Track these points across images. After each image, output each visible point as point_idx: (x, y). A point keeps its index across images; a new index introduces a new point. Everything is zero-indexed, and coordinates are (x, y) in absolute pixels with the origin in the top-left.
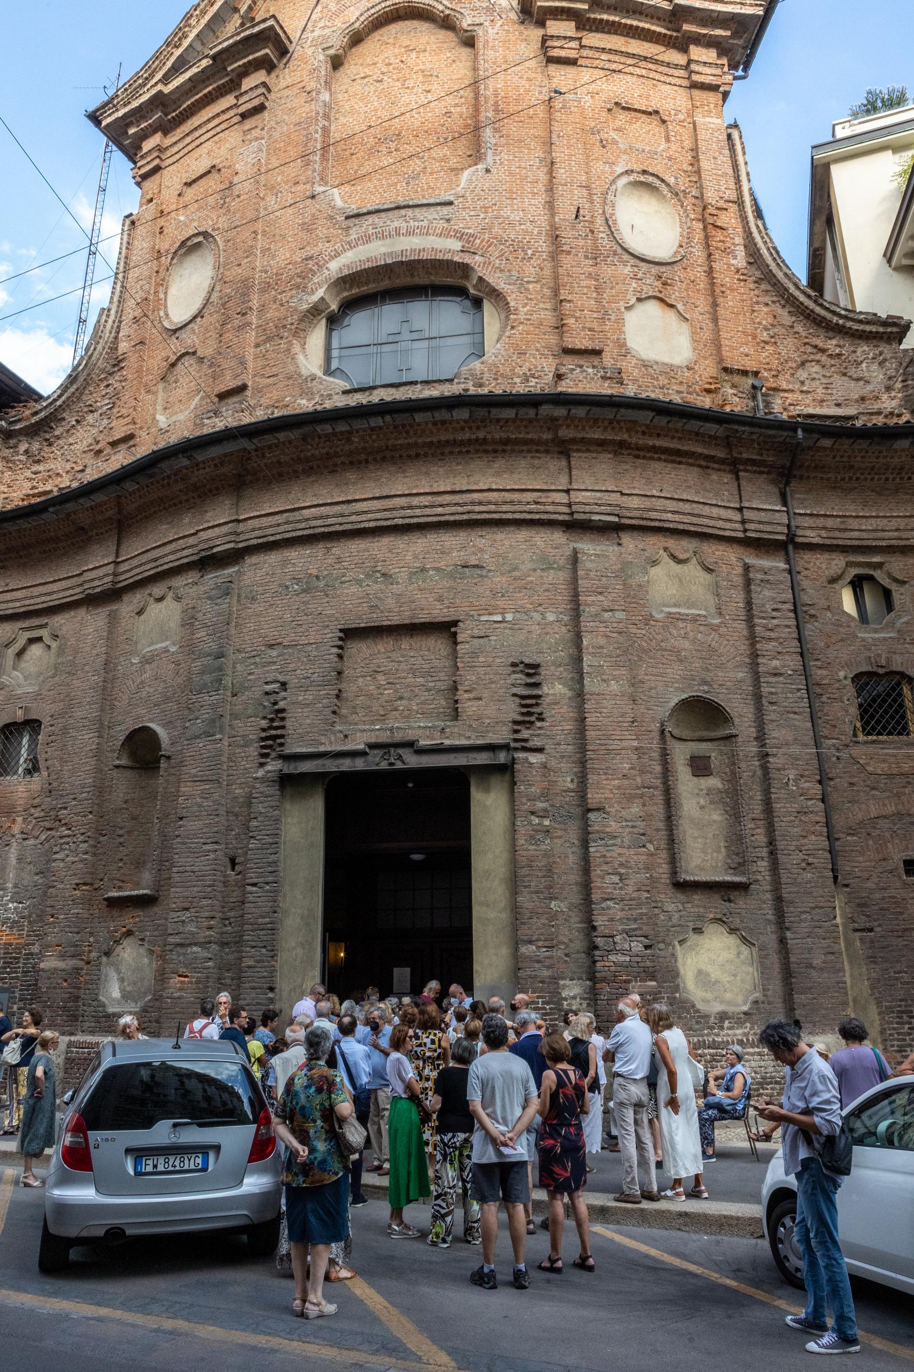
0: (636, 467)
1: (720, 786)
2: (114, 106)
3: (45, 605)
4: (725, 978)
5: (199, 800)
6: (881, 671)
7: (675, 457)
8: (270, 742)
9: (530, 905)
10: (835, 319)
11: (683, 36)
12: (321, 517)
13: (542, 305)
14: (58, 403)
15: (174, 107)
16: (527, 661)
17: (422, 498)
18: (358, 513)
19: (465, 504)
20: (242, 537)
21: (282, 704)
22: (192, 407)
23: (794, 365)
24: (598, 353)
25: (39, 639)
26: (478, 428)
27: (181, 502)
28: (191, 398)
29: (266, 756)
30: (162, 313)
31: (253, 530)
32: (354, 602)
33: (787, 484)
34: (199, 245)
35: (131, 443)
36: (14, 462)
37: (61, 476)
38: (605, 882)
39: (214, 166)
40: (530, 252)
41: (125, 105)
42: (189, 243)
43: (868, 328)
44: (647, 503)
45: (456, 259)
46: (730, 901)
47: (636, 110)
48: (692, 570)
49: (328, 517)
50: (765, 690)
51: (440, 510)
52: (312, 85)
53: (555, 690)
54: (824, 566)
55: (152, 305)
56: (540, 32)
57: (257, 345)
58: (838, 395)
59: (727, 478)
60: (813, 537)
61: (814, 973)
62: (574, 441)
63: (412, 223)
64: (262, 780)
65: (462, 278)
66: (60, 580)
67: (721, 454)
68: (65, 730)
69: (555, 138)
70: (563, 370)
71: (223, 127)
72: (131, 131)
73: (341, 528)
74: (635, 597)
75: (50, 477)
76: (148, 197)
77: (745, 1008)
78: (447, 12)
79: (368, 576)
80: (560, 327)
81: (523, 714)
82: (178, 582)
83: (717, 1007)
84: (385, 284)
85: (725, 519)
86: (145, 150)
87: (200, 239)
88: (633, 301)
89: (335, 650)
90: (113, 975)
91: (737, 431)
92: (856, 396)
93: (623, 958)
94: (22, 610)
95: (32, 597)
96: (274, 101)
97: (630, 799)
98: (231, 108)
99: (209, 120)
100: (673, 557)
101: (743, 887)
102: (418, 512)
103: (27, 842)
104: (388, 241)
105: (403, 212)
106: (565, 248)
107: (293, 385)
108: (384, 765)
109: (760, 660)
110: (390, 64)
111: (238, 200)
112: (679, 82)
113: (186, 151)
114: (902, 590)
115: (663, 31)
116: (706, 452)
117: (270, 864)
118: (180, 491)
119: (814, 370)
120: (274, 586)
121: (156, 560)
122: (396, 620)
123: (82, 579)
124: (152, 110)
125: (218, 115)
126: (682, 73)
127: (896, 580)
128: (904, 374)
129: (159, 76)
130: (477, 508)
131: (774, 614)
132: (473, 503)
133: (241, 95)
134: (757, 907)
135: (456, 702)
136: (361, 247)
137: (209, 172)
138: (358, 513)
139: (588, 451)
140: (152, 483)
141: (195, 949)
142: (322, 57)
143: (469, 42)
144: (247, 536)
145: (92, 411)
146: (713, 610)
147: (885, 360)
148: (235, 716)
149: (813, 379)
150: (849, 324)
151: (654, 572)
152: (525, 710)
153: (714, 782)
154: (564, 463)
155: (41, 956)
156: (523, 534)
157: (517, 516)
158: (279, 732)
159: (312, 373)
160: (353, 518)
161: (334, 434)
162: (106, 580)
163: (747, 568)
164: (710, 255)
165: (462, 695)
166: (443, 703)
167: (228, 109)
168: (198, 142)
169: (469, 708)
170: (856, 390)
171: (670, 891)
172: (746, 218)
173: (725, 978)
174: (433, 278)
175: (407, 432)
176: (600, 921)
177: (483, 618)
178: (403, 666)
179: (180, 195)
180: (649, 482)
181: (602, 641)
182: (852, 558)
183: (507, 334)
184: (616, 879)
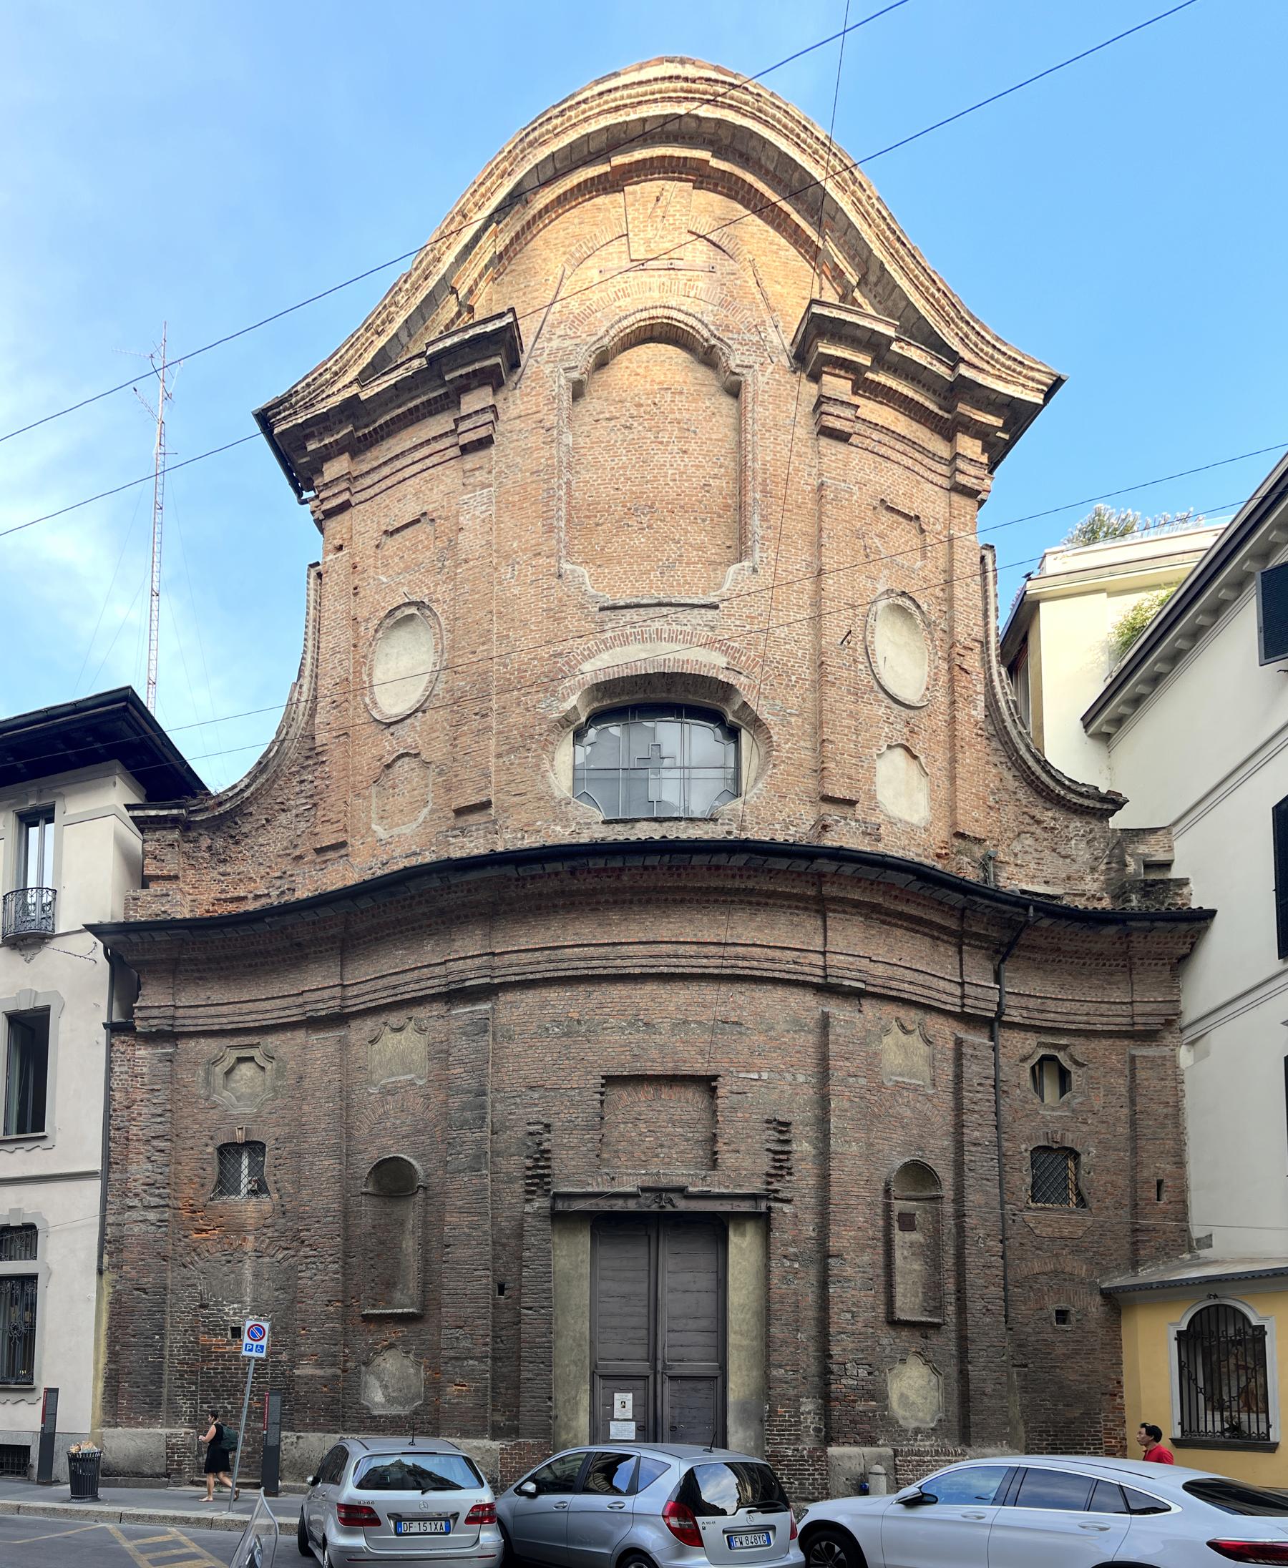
0: (881, 933)
1: (922, 1240)
2: (292, 406)
3: (257, 1024)
4: (919, 1401)
5: (466, 1230)
6: (1055, 1146)
7: (915, 925)
8: (537, 1180)
9: (780, 1336)
10: (1058, 789)
11: (954, 419)
12: (585, 959)
13: (802, 743)
14: (246, 794)
15: (365, 420)
16: (781, 1119)
17: (687, 947)
18: (622, 958)
19: (730, 958)
20: (497, 973)
21: (546, 1146)
22: (420, 820)
23: (1011, 836)
24: (851, 803)
25: (251, 1059)
26: (749, 877)
27: (421, 927)
28: (418, 809)
29: (533, 1192)
30: (367, 700)
31: (511, 966)
32: (617, 1048)
33: (1003, 961)
34: (411, 617)
35: (343, 852)
36: (196, 859)
37: (255, 882)
38: (839, 1318)
39: (424, 514)
40: (794, 678)
41: (306, 407)
42: (399, 615)
43: (1086, 802)
44: (890, 971)
45: (721, 677)
46: (926, 1338)
47: (898, 512)
48: (915, 1041)
49: (592, 958)
50: (967, 1157)
51: (705, 961)
52: (551, 420)
53: (803, 1147)
54: (1019, 1045)
55: (356, 686)
56: (811, 389)
57: (499, 756)
58: (1048, 872)
59: (952, 951)
60: (1014, 1016)
61: (986, 1400)
62: (835, 900)
63: (674, 626)
64: (535, 1215)
65: (720, 701)
66: (273, 998)
67: (952, 924)
68: (299, 1155)
69: (825, 540)
70: (829, 821)
71: (435, 459)
72: (312, 446)
73: (605, 972)
74: (873, 1063)
75: (241, 880)
76: (337, 542)
77: (933, 1425)
78: (713, 341)
79: (630, 1024)
80: (820, 772)
81: (775, 1168)
82: (420, 1012)
83: (913, 1424)
84: (639, 697)
85: (947, 993)
86: (327, 478)
87: (413, 610)
88: (884, 749)
89: (598, 1096)
90: (373, 1381)
91: (975, 903)
92: (1064, 875)
93: (851, 1382)
94: (230, 1027)
95: (241, 1014)
96: (502, 434)
97: (862, 1249)
98: (445, 435)
99: (415, 448)
100: (902, 1027)
101: (936, 1326)
102: (683, 961)
103: (260, 1260)
104: (648, 645)
105: (665, 610)
106: (830, 678)
107: (545, 807)
108: (654, 1208)
109: (965, 1131)
110: (641, 405)
111: (465, 566)
112: (940, 480)
113: (383, 485)
114: (1080, 1072)
115: (936, 410)
116: (942, 922)
117: (544, 1291)
118: (424, 914)
119: (1027, 842)
120: (533, 1027)
121: (394, 987)
122: (659, 1070)
123: (300, 1000)
124: (341, 422)
125: (428, 442)
126: (944, 469)
127: (1076, 1063)
128: (1110, 856)
129: (353, 373)
130: (741, 963)
131: (979, 1088)
132: (737, 957)
133: (463, 418)
134: (945, 1342)
135: (716, 1153)
136: (618, 649)
137: (418, 521)
138: (622, 958)
139: (844, 912)
140: (391, 903)
141: (471, 1362)
142: (563, 381)
143: (734, 391)
144: (503, 972)
145: (283, 810)
146: (928, 1081)
147: (1095, 838)
148: (496, 1153)
149: (1026, 852)
150: (1070, 796)
151: (886, 1040)
152: (778, 1164)
153: (916, 1236)
154: (820, 923)
155: (294, 1363)
156: (780, 993)
157: (777, 975)
158: (546, 1171)
159: (560, 796)
160: (618, 962)
161: (605, 870)
162: (331, 1003)
163: (959, 1043)
164: (953, 702)
165: (720, 1147)
166: (701, 1153)
167: (441, 436)
168: (400, 476)
169: (727, 1159)
170: (1063, 869)
171: (886, 1328)
172: (989, 662)
173: (919, 1401)
174: (690, 697)
175: (679, 875)
176: (835, 1351)
177: (742, 1075)
178: (663, 1116)
179: (377, 546)
180: (891, 951)
181: (846, 1105)
182: (1044, 1039)
183: (769, 773)
184: (849, 1316)
